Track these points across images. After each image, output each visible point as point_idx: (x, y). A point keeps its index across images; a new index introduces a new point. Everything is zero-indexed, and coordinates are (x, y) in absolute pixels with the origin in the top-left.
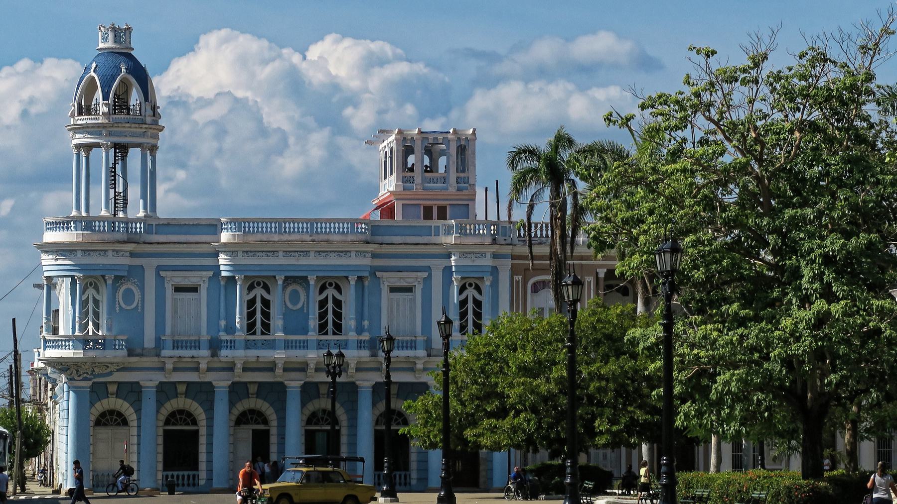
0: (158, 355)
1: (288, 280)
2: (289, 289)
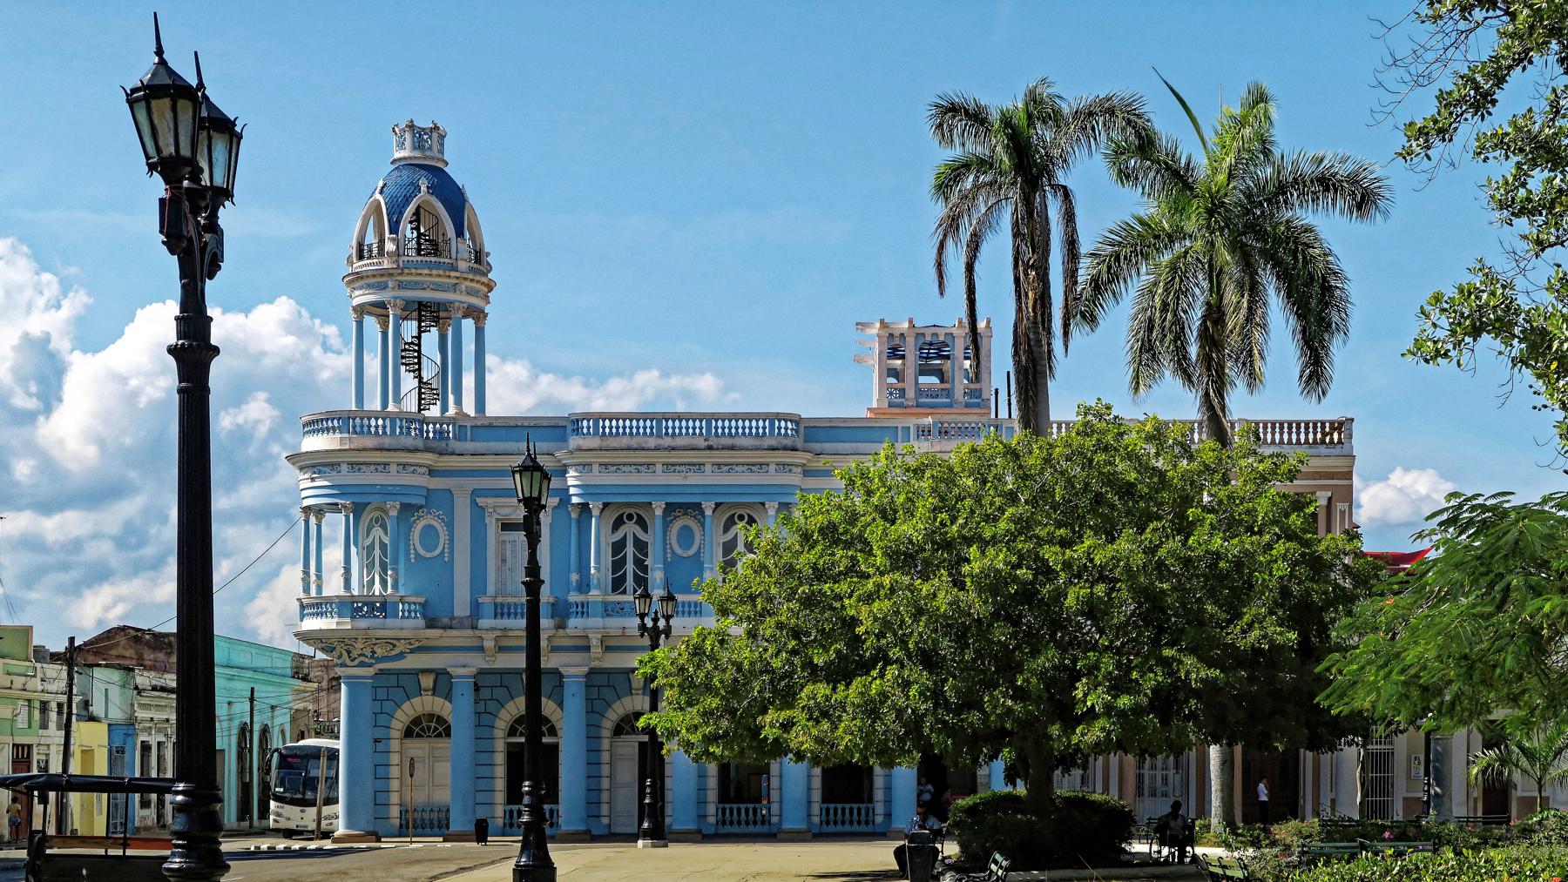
0: (474, 627)
1: (670, 508)
2: (677, 526)
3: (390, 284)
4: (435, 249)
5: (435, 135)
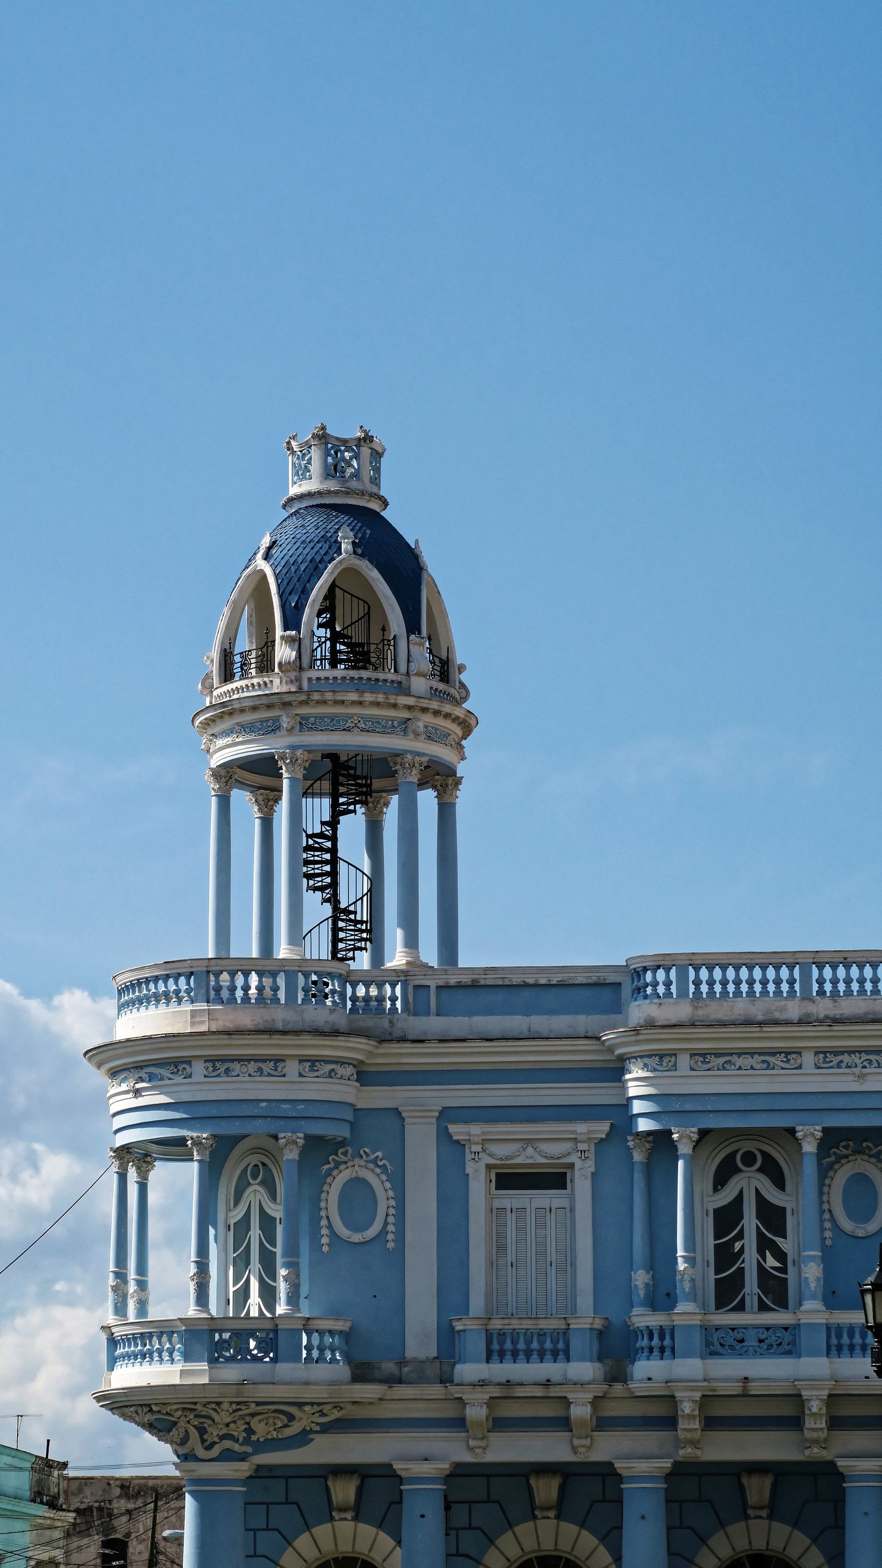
0: (446, 1379)
1: (832, 1139)
3: (285, 722)
4: (361, 657)
5: (365, 451)
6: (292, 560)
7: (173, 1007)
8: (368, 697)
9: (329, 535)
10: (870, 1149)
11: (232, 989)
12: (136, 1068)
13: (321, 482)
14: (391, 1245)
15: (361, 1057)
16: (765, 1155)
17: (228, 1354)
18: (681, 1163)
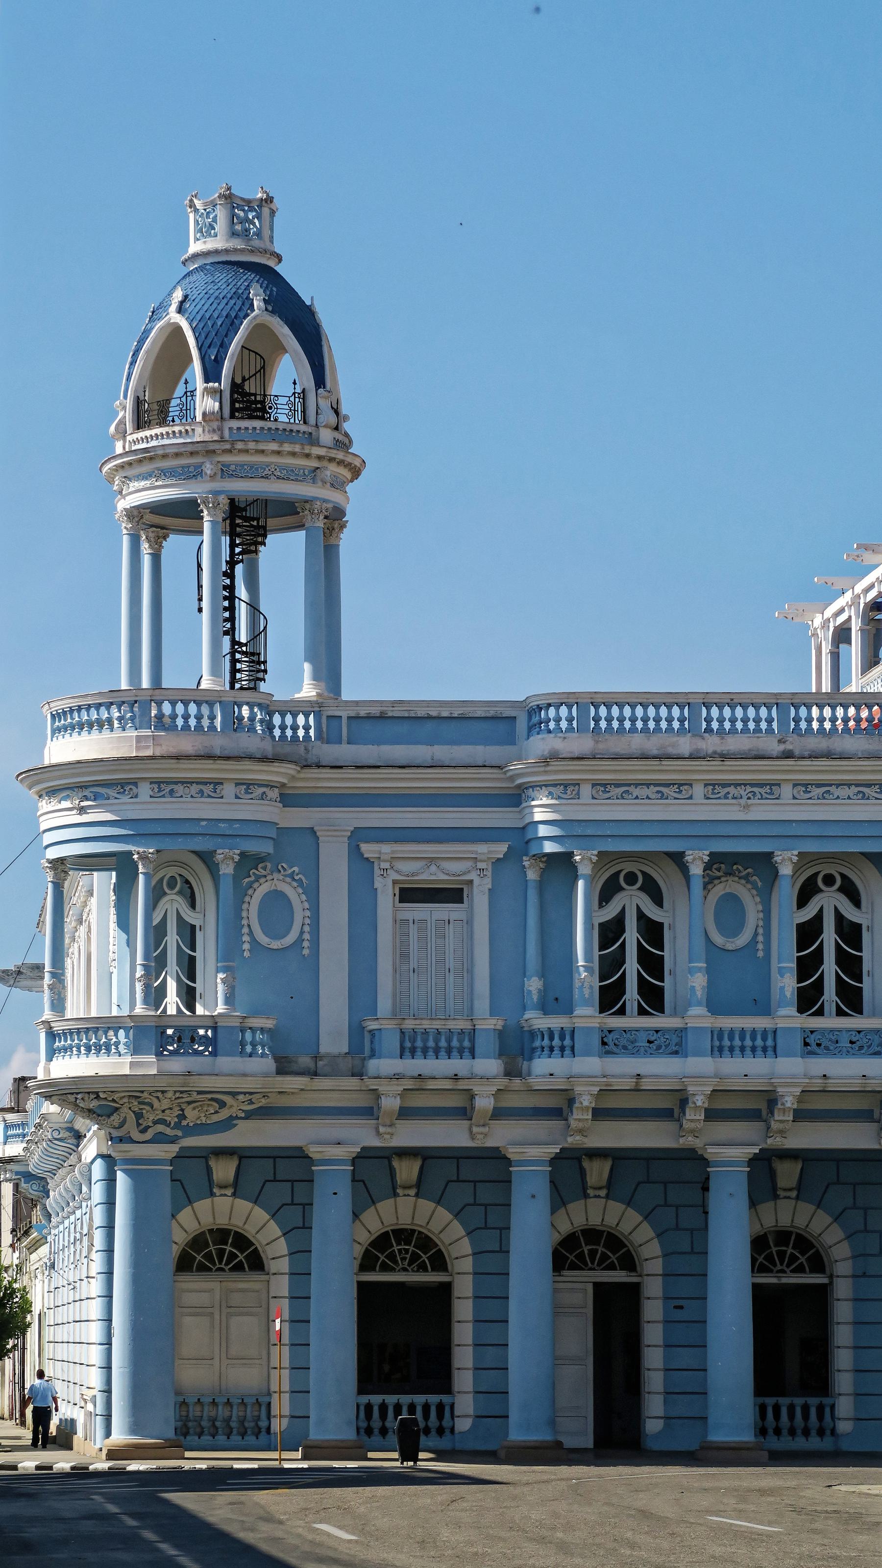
0: (358, 1073)
1: (716, 860)
2: (719, 890)
3: (208, 469)
6: (207, 315)
7: (106, 733)
8: (287, 447)
9: (240, 291)
10: (740, 872)
11: (174, 716)
12: (81, 787)
13: (227, 241)
14: (306, 952)
15: (285, 781)
16: (843, 876)
17: (171, 1048)
18: (581, 884)
